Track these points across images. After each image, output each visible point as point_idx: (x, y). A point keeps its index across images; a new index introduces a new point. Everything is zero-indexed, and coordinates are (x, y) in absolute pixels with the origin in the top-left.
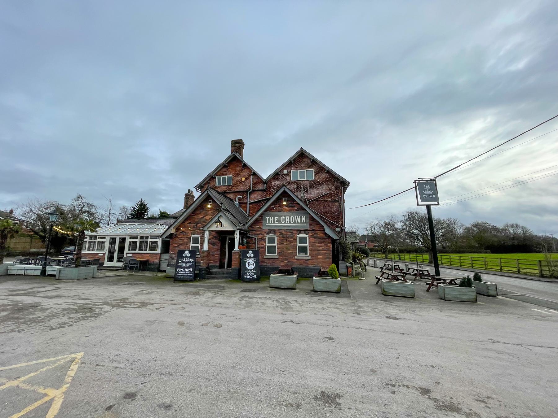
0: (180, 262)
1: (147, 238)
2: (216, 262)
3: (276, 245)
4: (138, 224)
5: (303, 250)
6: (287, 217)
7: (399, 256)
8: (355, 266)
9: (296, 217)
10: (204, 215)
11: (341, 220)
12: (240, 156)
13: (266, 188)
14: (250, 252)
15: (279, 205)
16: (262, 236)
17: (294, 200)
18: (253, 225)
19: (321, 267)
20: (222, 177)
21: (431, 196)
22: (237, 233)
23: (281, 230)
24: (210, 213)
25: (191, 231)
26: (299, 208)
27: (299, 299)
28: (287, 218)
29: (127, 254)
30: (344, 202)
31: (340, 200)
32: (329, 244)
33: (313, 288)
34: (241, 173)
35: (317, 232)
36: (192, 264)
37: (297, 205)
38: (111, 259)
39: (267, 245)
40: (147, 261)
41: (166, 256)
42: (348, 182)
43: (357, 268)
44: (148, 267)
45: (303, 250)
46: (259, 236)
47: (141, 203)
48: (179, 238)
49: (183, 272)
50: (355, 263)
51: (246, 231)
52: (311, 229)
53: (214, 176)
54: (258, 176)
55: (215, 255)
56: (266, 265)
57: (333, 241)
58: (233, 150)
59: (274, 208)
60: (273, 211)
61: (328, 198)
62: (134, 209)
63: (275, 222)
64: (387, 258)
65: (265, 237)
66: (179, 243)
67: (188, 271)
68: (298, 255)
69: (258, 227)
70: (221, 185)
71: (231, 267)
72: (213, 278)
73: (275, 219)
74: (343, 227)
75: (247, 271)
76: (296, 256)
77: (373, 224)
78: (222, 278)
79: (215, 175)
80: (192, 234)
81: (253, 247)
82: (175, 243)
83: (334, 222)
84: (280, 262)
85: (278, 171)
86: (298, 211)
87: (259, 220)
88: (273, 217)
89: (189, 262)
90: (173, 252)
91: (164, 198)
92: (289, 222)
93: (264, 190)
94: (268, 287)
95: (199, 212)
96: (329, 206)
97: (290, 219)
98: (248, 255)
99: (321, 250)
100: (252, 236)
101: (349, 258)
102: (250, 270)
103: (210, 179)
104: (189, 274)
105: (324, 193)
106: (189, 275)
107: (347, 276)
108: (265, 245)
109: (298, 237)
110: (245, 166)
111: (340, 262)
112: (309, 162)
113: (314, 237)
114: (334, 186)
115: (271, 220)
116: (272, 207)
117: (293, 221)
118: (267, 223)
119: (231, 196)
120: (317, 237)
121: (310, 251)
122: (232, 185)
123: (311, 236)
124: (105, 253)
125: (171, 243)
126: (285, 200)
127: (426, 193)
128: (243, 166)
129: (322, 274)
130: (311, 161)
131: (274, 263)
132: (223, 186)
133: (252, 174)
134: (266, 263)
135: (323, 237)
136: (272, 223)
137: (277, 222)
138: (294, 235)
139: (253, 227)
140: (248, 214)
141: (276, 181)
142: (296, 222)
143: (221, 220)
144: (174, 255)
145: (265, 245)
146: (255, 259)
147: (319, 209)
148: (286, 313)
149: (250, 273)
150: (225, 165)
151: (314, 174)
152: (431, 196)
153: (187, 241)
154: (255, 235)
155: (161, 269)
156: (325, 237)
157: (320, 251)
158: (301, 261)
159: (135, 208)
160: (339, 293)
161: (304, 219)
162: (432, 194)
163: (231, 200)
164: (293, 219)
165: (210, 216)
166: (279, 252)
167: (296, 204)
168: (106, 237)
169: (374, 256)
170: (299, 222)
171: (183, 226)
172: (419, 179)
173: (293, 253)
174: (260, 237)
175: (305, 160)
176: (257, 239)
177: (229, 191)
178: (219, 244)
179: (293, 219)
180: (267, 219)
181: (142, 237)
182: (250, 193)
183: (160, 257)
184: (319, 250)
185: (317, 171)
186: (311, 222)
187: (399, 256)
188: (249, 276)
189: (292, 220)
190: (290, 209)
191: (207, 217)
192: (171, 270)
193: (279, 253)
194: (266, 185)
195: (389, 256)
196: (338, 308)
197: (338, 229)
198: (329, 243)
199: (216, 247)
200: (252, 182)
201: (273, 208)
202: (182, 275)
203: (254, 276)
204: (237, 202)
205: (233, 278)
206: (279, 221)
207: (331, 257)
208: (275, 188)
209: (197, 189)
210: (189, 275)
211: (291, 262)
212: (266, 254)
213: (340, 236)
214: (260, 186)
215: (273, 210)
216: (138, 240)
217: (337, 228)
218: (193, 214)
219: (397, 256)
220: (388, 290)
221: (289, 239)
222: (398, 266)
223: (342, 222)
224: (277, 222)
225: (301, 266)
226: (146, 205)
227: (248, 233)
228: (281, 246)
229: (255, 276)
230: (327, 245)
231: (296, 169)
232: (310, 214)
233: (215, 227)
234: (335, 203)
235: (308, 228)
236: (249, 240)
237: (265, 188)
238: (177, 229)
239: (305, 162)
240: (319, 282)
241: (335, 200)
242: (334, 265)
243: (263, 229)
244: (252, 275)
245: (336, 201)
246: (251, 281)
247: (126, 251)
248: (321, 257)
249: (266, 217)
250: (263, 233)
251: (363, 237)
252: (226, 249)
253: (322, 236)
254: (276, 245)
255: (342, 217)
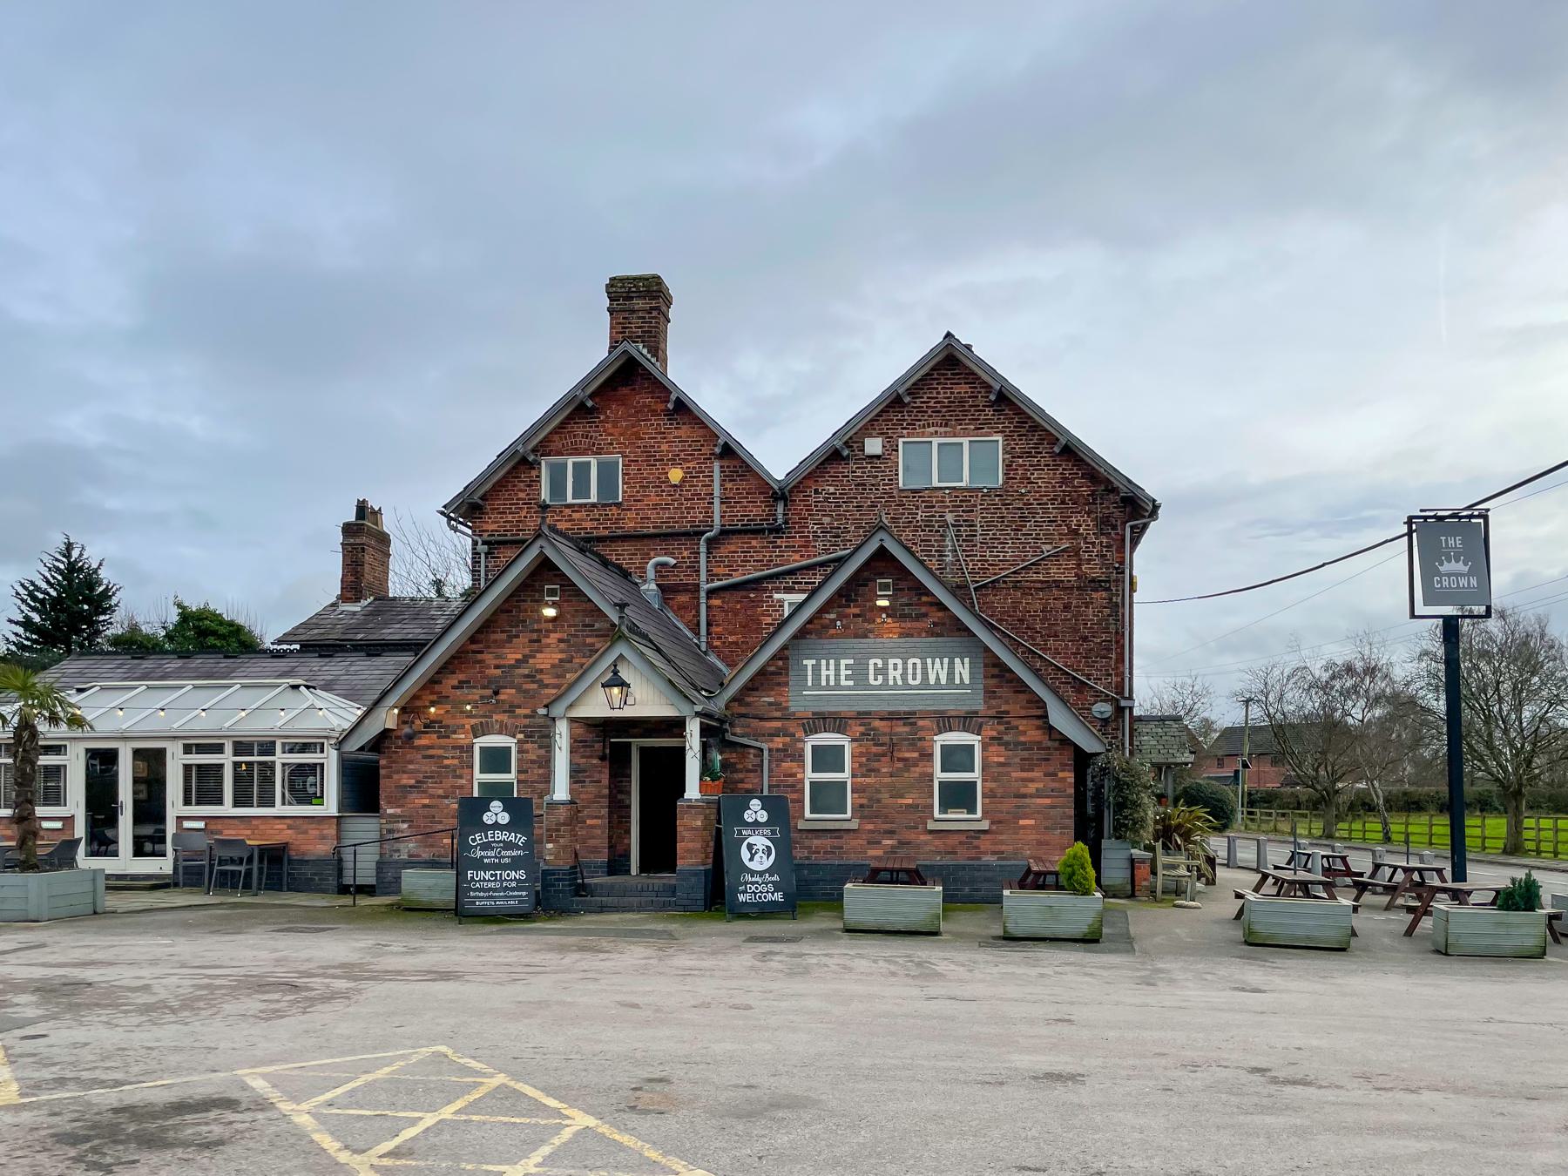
0: (476, 847)
1: (268, 749)
2: (595, 850)
3: (845, 776)
4: (195, 687)
5: (958, 796)
6: (891, 662)
7: (1385, 824)
8: (1162, 859)
9: (929, 661)
10: (527, 651)
11: (1117, 668)
12: (653, 360)
13: (786, 522)
14: (755, 804)
15: (856, 611)
16: (788, 739)
17: (921, 589)
18: (749, 696)
19: (1031, 861)
20: (570, 461)
21: (1463, 582)
22: (693, 728)
23: (869, 713)
24: (555, 641)
25: (473, 721)
26: (944, 624)
27: (962, 956)
28: (891, 666)
29: (180, 819)
30: (1132, 589)
31: (1117, 581)
32: (1063, 771)
33: (1005, 927)
34: (664, 447)
35: (1015, 722)
36: (520, 853)
37: (934, 608)
38: (102, 842)
39: (810, 775)
40: (284, 847)
41: (364, 828)
42: (1154, 501)
43: (1174, 867)
44: (289, 874)
45: (958, 796)
46: (777, 739)
47: (69, 563)
48: (418, 748)
49: (491, 885)
50: (1165, 847)
51: (722, 721)
52: (992, 712)
53: (531, 458)
54: (744, 462)
55: (588, 822)
56: (807, 858)
57: (1082, 760)
58: (620, 333)
59: (839, 623)
60: (832, 637)
61: (1063, 572)
62: (31, 594)
63: (843, 683)
64: (1330, 836)
65: (800, 745)
66: (418, 771)
67: (511, 880)
68: (937, 815)
69: (770, 704)
70: (570, 500)
71: (671, 866)
72: (602, 909)
73: (842, 667)
74: (1126, 699)
75: (748, 878)
76: (929, 821)
77: (1276, 672)
78: (640, 909)
79: (534, 451)
80: (478, 731)
81: (750, 786)
82: (404, 772)
83: (1088, 676)
84: (865, 843)
85: (838, 444)
86: (938, 635)
87: (773, 673)
88: (832, 662)
89: (508, 845)
90: (399, 811)
91: (113, 503)
92: (900, 683)
93: (777, 530)
94: (837, 929)
95: (504, 636)
96: (1067, 607)
97: (905, 669)
98: (748, 816)
99: (1031, 796)
100: (745, 741)
101: (1142, 827)
102: (757, 872)
103: (514, 468)
104: (513, 889)
105: (1045, 547)
106: (516, 893)
107: (1132, 896)
108: (799, 776)
109: (939, 744)
110: (683, 410)
111: (1105, 843)
112: (981, 402)
113: (1006, 744)
114: (1093, 516)
115: (824, 673)
116: (827, 616)
117: (919, 677)
118: (810, 684)
119: (622, 555)
120: (1017, 744)
121: (987, 801)
122: (620, 504)
123: (992, 738)
124: (73, 816)
125: (382, 772)
126: (885, 587)
127: (1447, 567)
128: (669, 414)
129: (1033, 881)
130: (992, 397)
131: (842, 848)
132: (581, 505)
133: (717, 450)
134: (806, 848)
135: (1039, 743)
136: (828, 687)
137: (851, 683)
138: (921, 734)
139: (748, 704)
140: (704, 639)
141: (832, 490)
142: (932, 681)
143: (625, 674)
144: (403, 822)
145: (799, 776)
146: (773, 832)
147: (1021, 621)
148: (927, 984)
149: (757, 883)
150: (582, 405)
151: (1004, 460)
152: (1463, 582)
153: (456, 762)
154: (760, 735)
155: (348, 881)
156: (1049, 744)
157: (1027, 801)
158: (953, 841)
159: (38, 589)
160: (1097, 941)
161: (963, 670)
162: (1469, 574)
163: (626, 575)
164: (919, 671)
165: (554, 656)
166: (862, 806)
167: (931, 604)
168: (65, 746)
169: (1276, 830)
170: (943, 681)
171: (434, 697)
172: (1422, 511)
173: (917, 806)
174: (779, 742)
175: (963, 389)
176: (766, 753)
177: (606, 533)
178: (603, 776)
179: (919, 671)
180: (810, 668)
181: (241, 748)
182: (710, 542)
183: (339, 830)
184: (1024, 796)
185: (1020, 445)
186: (993, 681)
187: (1385, 824)
188: (755, 894)
189: (914, 674)
190: (903, 625)
191: (546, 659)
192: (422, 881)
193: (859, 809)
194: (786, 505)
195: (1340, 825)
196: (1086, 974)
197: (1103, 709)
198: (1063, 767)
199: (592, 789)
200: (717, 493)
201: (834, 621)
202: (489, 897)
203: (773, 894)
204: (653, 586)
205: (685, 908)
206: (859, 674)
207: (1071, 823)
208: (826, 520)
209: (450, 519)
210: (516, 893)
211: (909, 843)
212: (808, 814)
213: (1106, 741)
214: (756, 511)
215: (832, 631)
216: (227, 759)
217: (1096, 702)
218: (474, 647)
219: (1374, 826)
220: (1262, 928)
221: (899, 750)
222: (1343, 859)
223: (1119, 679)
224: (851, 683)
225: (948, 861)
226: (95, 571)
227: (727, 726)
228: (868, 780)
229: (778, 897)
230: (1056, 775)
231: (923, 435)
232: (987, 649)
233: (598, 705)
234: (1094, 595)
235: (979, 705)
236: (734, 755)
237: (780, 522)
238: (408, 710)
239: (962, 401)
240: (1023, 907)
241: (1093, 581)
242: (1080, 844)
243: (792, 709)
244: (767, 892)
245: (1096, 584)
246: (765, 912)
247: (174, 804)
248: (1032, 822)
249: (805, 662)
250: (792, 727)
251: (1229, 733)
252: (629, 793)
253: (1037, 739)
254: (845, 776)
255: (1123, 654)
